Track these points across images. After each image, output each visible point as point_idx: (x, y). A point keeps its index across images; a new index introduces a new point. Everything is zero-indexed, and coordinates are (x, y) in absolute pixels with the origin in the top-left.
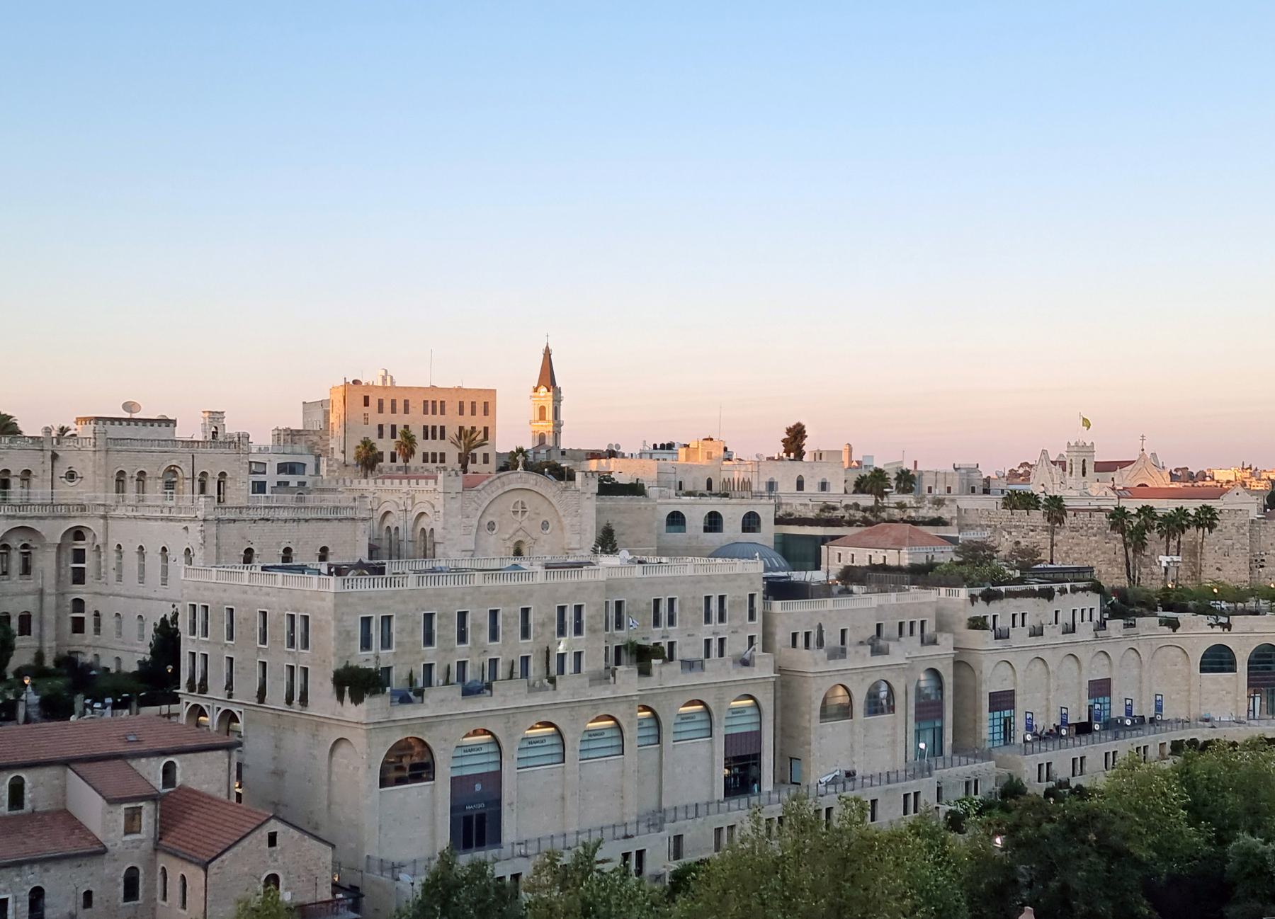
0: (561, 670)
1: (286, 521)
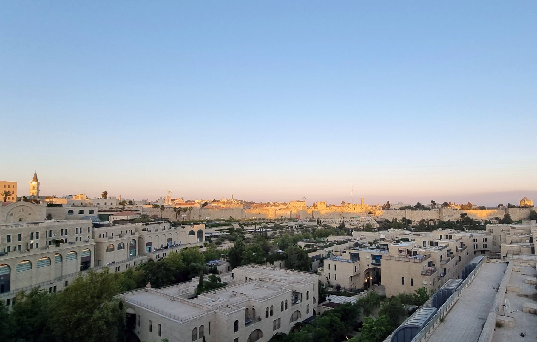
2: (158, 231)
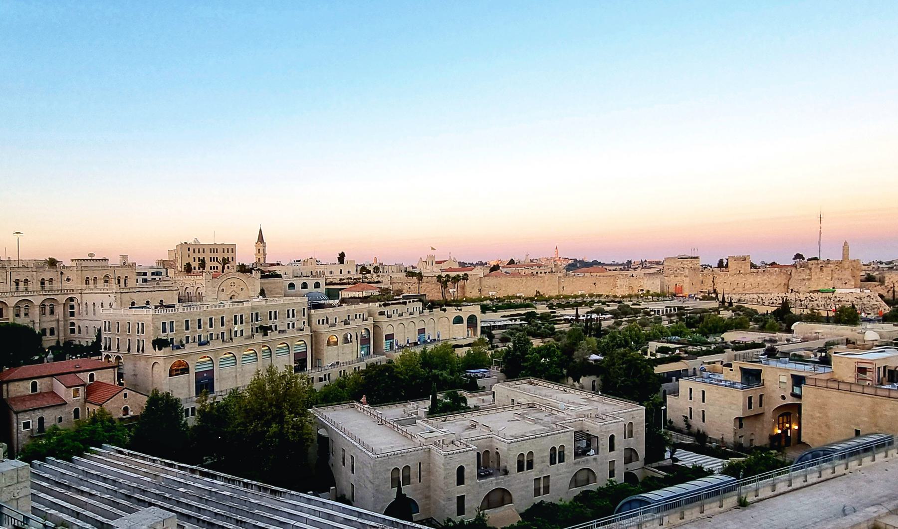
0: (236, 336)
1: (146, 292)
2: (402, 315)
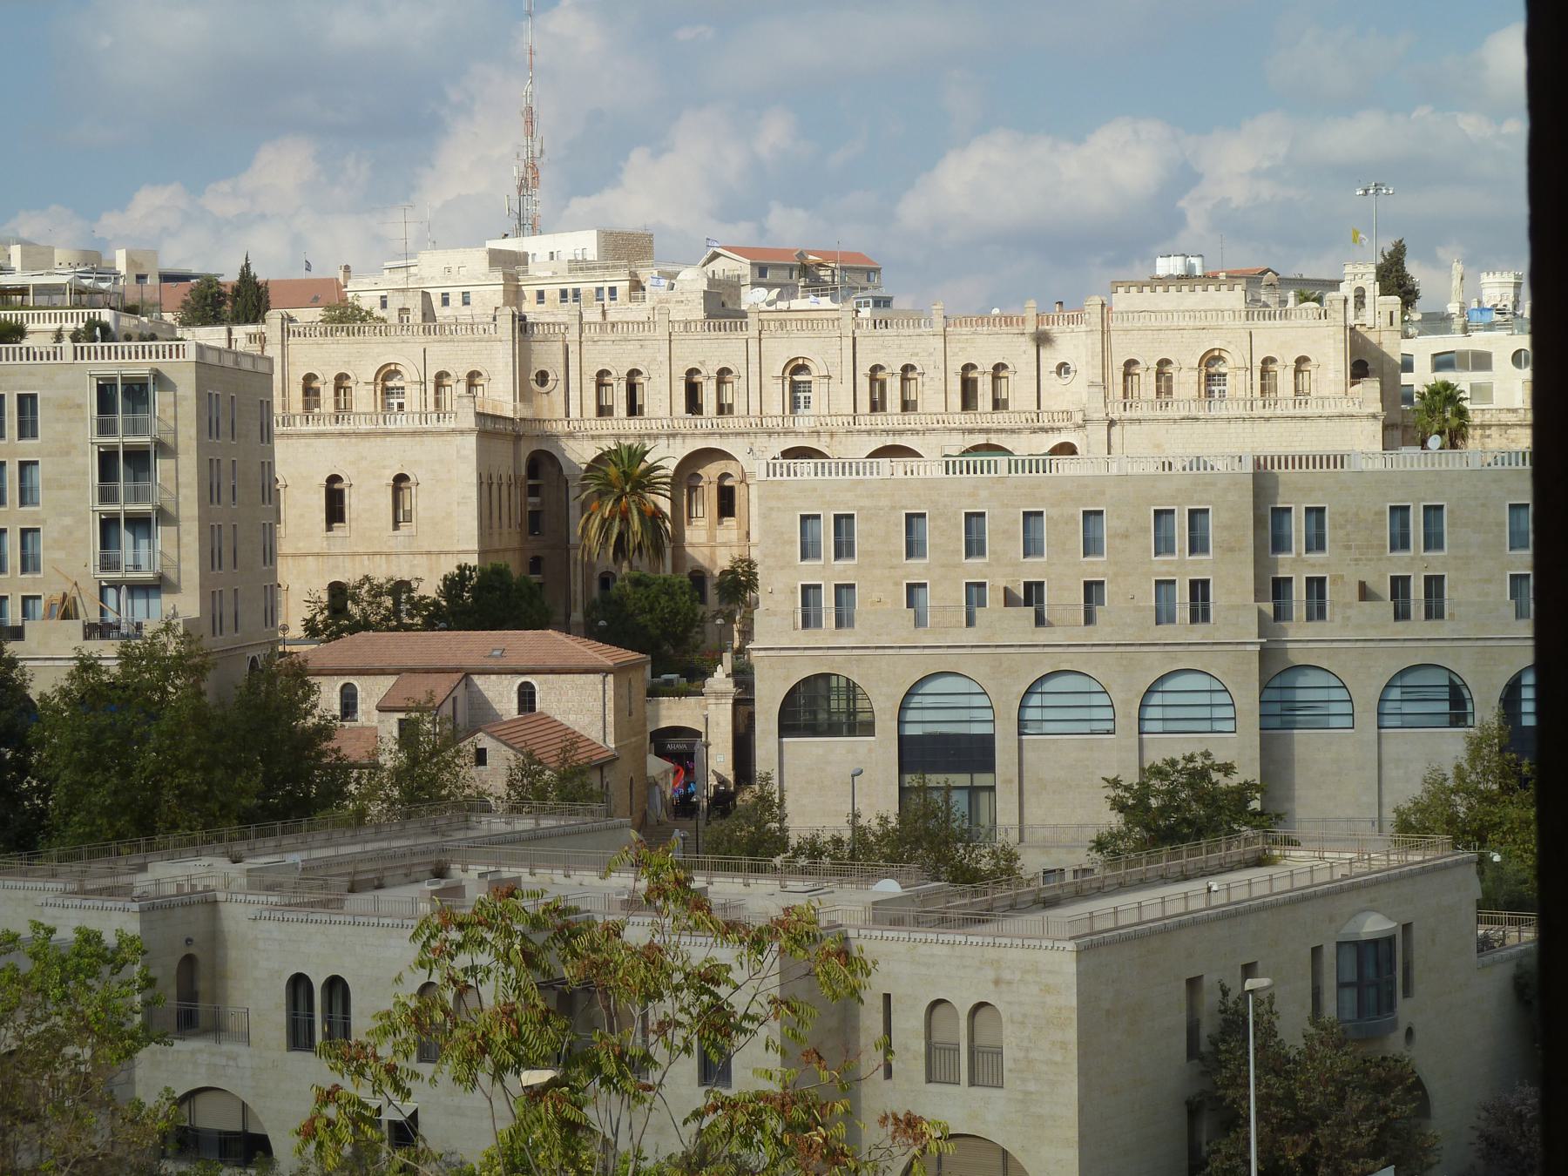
1: (1229, 420)
